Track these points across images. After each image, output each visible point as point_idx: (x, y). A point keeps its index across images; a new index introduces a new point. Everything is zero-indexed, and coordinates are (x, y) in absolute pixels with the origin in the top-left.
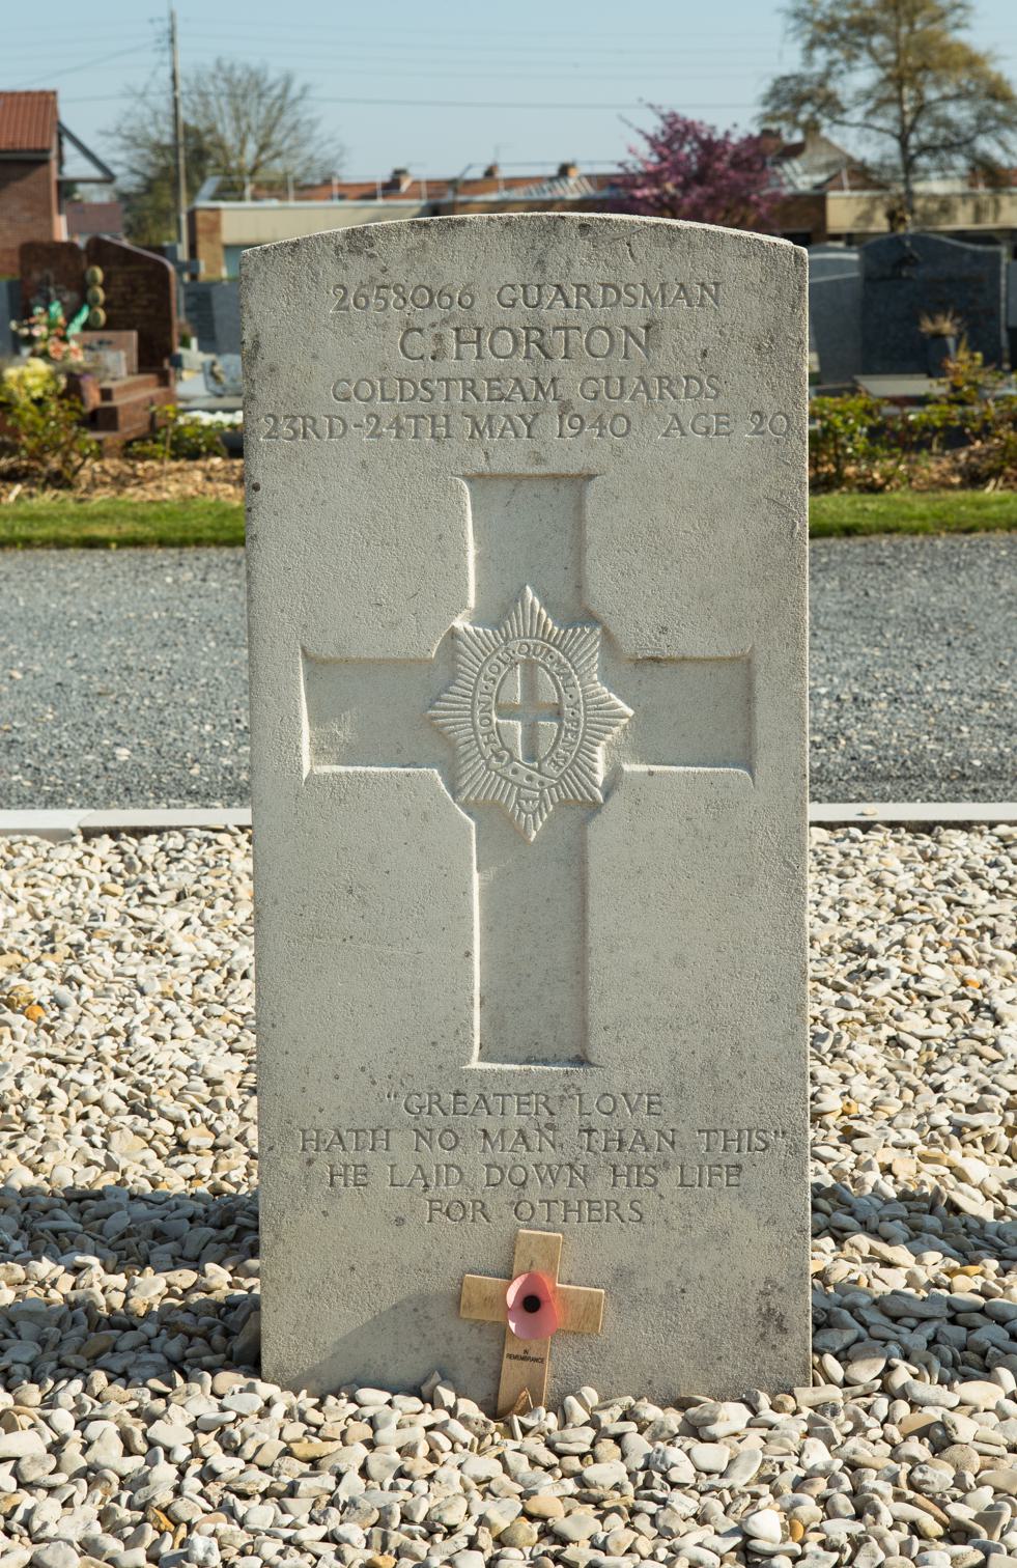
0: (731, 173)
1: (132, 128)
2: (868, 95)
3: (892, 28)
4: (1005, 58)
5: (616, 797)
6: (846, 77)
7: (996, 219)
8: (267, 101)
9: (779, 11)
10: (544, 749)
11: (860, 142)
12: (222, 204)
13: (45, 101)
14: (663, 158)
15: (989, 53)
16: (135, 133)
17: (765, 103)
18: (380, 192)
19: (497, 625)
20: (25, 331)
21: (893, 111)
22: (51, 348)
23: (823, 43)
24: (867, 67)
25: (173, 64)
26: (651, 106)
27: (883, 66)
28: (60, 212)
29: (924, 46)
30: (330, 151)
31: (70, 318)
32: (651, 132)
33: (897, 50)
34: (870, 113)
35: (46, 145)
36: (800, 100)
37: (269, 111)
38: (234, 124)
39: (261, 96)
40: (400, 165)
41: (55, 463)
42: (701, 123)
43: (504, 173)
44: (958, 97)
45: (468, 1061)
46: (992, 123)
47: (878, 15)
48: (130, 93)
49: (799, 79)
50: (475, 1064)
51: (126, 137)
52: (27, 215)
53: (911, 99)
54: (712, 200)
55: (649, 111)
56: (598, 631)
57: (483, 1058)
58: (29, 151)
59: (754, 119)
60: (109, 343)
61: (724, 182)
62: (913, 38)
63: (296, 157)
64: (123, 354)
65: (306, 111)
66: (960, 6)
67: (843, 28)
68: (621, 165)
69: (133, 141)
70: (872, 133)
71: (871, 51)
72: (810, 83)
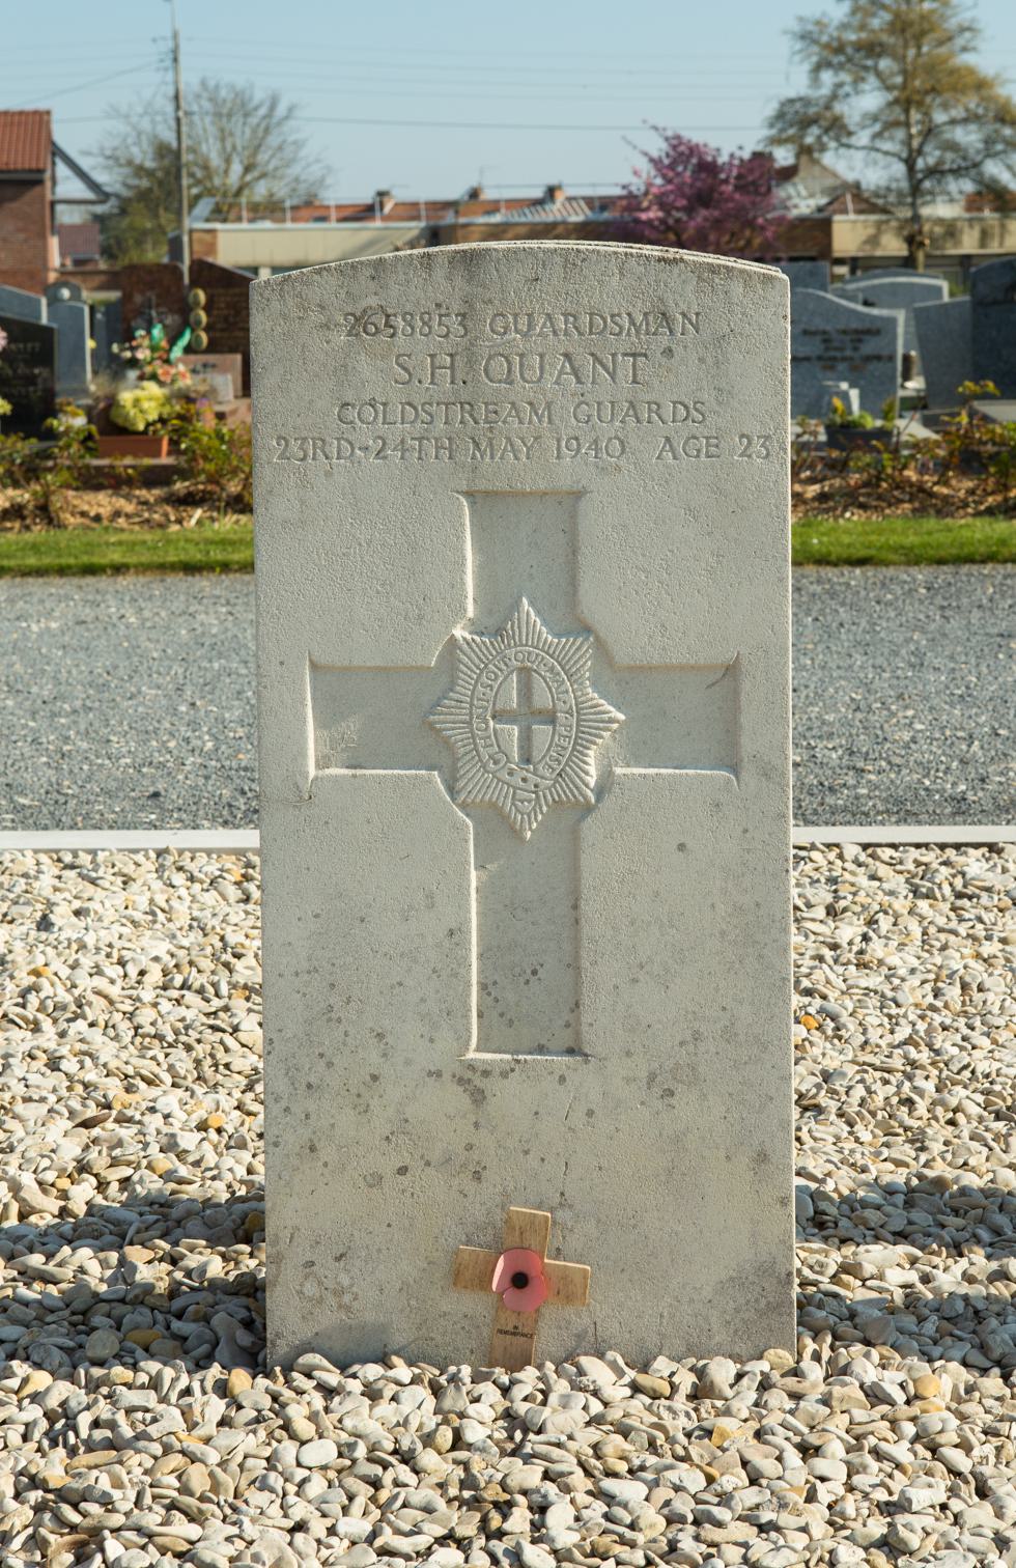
0: (737, 196)
1: (115, 149)
2: (875, 118)
3: (900, 51)
5: (609, 801)
6: (853, 100)
7: (1001, 244)
8: (253, 121)
9: (785, 32)
11: (867, 165)
12: (218, 226)
13: (38, 122)
14: (669, 181)
15: (997, 76)
17: (771, 126)
20: (128, 354)
21: (900, 134)
22: (160, 371)
23: (829, 65)
25: (176, 83)
26: (655, 128)
27: (889, 88)
28: (53, 233)
29: (931, 69)
30: (316, 171)
31: (172, 341)
32: (655, 154)
33: (904, 72)
34: (877, 136)
35: (41, 166)
36: (806, 123)
37: (254, 131)
38: (218, 145)
39: (246, 115)
40: (383, 187)
41: (234, 487)
42: (705, 145)
43: (488, 195)
44: (965, 121)
46: (999, 147)
47: (885, 38)
48: (114, 112)
51: (108, 158)
52: (21, 236)
53: (918, 122)
54: (717, 223)
55: (653, 132)
58: (24, 171)
60: (214, 366)
61: (731, 205)
62: (920, 61)
63: (281, 178)
64: (230, 377)
66: (969, 29)
67: (849, 50)
68: (624, 187)
69: (113, 159)
70: (879, 156)
71: (879, 74)
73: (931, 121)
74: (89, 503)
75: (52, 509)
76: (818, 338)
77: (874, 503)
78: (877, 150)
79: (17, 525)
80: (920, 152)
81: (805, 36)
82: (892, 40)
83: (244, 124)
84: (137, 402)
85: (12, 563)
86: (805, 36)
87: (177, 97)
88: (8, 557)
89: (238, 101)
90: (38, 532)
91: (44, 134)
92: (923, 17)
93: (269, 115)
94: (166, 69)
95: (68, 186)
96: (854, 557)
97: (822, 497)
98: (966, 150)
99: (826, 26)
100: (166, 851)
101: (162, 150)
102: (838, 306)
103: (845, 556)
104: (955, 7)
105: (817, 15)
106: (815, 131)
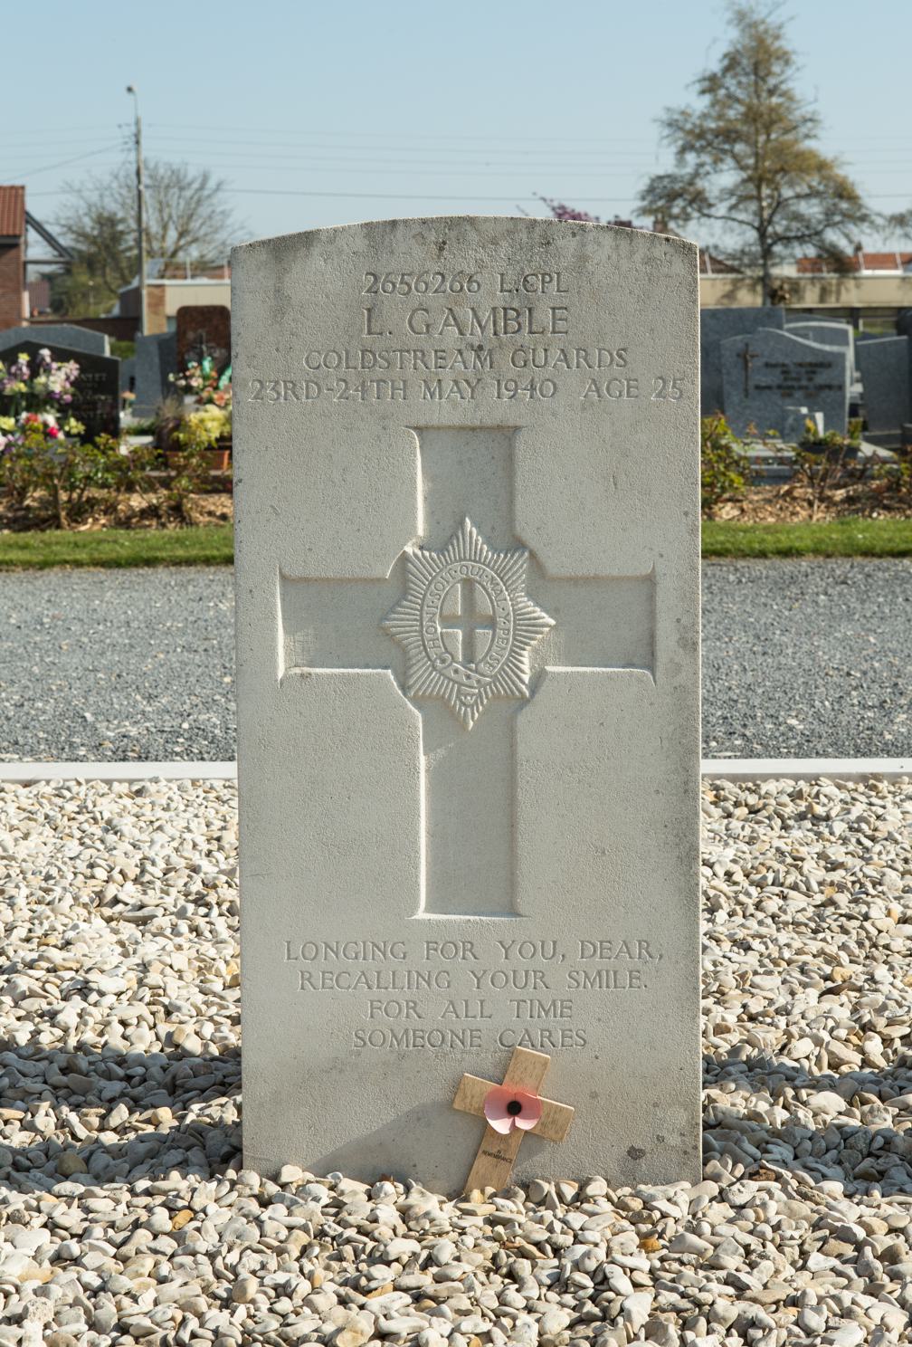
2: (732, 193)
6: (714, 177)
8: (188, 193)
9: (655, 121)
11: (725, 232)
12: (166, 282)
13: (16, 193)
15: (836, 158)
16: (71, 222)
17: (643, 198)
19: (442, 550)
20: (183, 382)
21: (753, 206)
26: (544, 200)
27: (743, 168)
29: (780, 151)
33: (756, 155)
35: (17, 232)
36: (672, 196)
37: (188, 203)
38: (157, 214)
39: (182, 189)
44: (807, 196)
46: (837, 218)
47: (739, 126)
48: (69, 188)
49: (672, 178)
50: (421, 914)
51: (63, 226)
55: (541, 202)
56: (526, 554)
57: (427, 910)
59: (633, 212)
65: (222, 202)
66: (811, 120)
70: (735, 224)
71: (735, 157)
72: (681, 181)
73: (780, 195)
74: (214, 504)
75: (184, 508)
76: (778, 370)
77: (897, 505)
78: (734, 220)
79: (154, 523)
80: (770, 222)
81: (671, 124)
82: (745, 128)
83: (179, 197)
85: (164, 554)
86: (671, 124)
88: (159, 549)
89: (174, 178)
90: (173, 529)
91: (19, 201)
92: (772, 110)
93: (202, 188)
94: (129, 150)
95: (36, 249)
96: (896, 550)
97: (849, 500)
98: (809, 221)
99: (690, 115)
101: (106, 222)
102: (795, 342)
103: (887, 549)
104: (799, 102)
105: (683, 107)
106: (680, 203)
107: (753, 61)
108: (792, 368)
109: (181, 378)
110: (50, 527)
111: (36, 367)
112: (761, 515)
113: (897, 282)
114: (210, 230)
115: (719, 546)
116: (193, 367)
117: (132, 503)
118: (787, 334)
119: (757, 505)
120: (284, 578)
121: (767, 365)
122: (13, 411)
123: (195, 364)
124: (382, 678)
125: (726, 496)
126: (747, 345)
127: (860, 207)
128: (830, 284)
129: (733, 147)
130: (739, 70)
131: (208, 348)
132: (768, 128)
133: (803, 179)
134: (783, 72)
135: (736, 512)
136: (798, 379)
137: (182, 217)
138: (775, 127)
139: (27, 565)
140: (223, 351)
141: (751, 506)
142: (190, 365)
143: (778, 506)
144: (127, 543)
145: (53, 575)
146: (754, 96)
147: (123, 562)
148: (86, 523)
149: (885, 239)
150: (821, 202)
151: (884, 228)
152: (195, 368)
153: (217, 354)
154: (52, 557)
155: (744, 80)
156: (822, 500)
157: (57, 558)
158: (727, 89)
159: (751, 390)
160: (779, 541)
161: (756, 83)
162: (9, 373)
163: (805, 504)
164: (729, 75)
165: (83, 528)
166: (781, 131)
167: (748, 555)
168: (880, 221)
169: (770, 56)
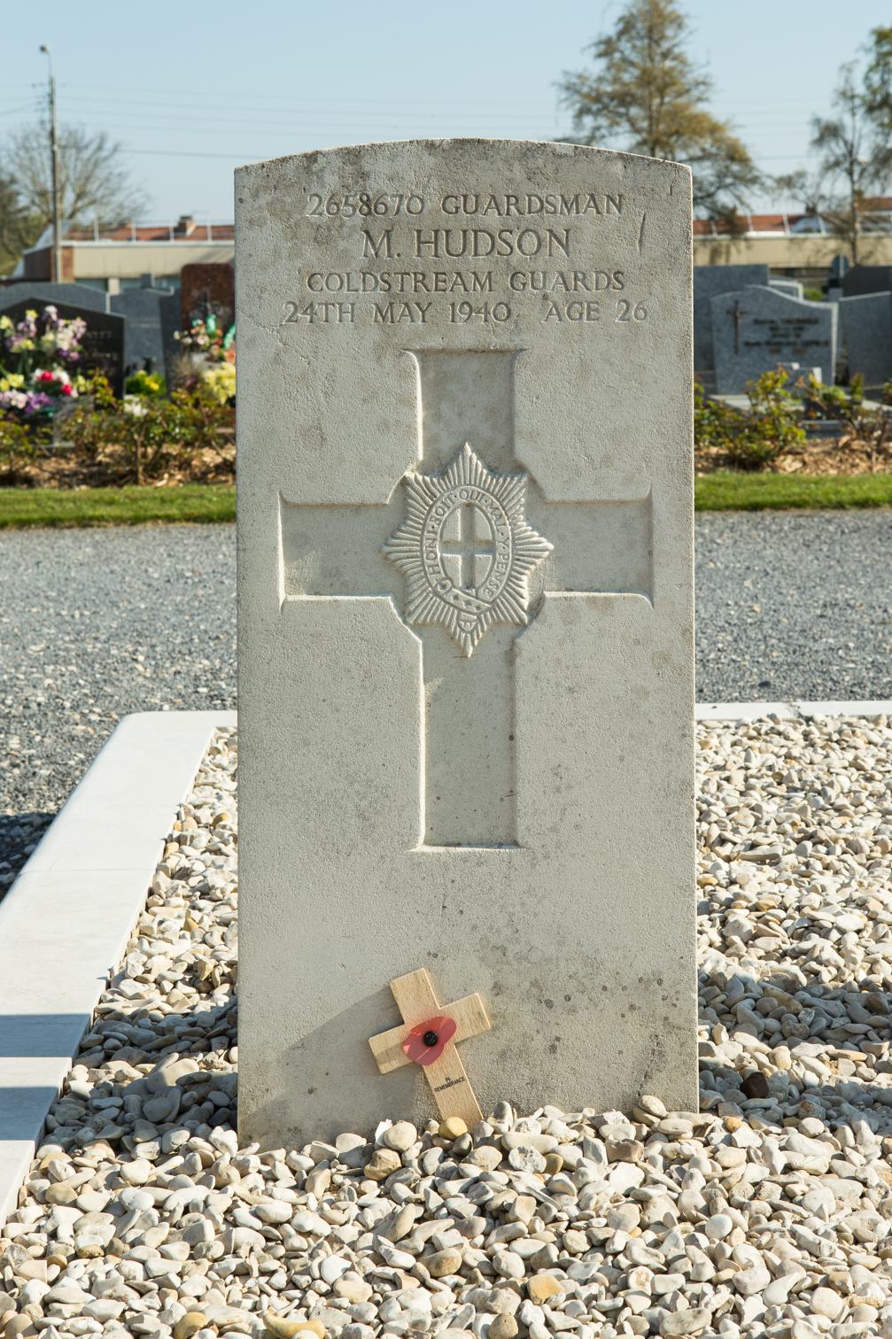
4: (741, 126)
8: (86, 154)
9: (553, 84)
10: (479, 581)
12: (74, 243)
18: (172, 234)
20: (189, 340)
24: (625, 132)
27: (637, 131)
29: (675, 113)
33: (650, 118)
37: (85, 165)
39: (79, 149)
40: (186, 213)
45: (408, 843)
46: (729, 180)
47: (634, 90)
56: (525, 479)
57: (427, 843)
62: (664, 108)
63: (107, 204)
65: (120, 163)
66: (704, 83)
71: (632, 122)
76: (767, 327)
81: (569, 88)
83: (77, 159)
84: (219, 380)
86: (569, 88)
87: (52, 134)
92: (667, 73)
93: (100, 148)
94: (43, 110)
99: (587, 79)
100: (204, 760)
105: (580, 70)
107: (647, 24)
108: (781, 325)
109: (186, 336)
110: (126, 483)
111: (43, 324)
112: (823, 467)
113: (786, 243)
114: (107, 192)
115: (797, 498)
116: (198, 325)
117: (206, 459)
118: (775, 291)
119: (817, 457)
120: (285, 503)
121: (756, 322)
122: (20, 369)
123: (200, 322)
124: (381, 605)
125: (787, 449)
126: (737, 302)
127: (751, 169)
128: (720, 245)
129: (628, 109)
130: (633, 33)
131: (213, 306)
132: (662, 92)
133: (696, 142)
134: (676, 35)
135: (798, 465)
136: (786, 336)
137: (80, 178)
138: (668, 91)
139: (119, 521)
140: (228, 309)
141: (812, 459)
142: (194, 323)
143: (838, 458)
144: (215, 499)
145: (149, 531)
146: (648, 60)
147: (215, 517)
148: (162, 479)
149: (774, 201)
150: (713, 165)
151: (773, 189)
152: (200, 326)
153: (221, 312)
154: (142, 513)
155: (638, 43)
156: (879, 452)
157: (149, 513)
158: (622, 52)
159: (741, 347)
160: (853, 493)
161: (650, 46)
162: (17, 331)
163: (864, 456)
164: (624, 38)
165: (160, 484)
166: (673, 95)
167: (826, 507)
168: (769, 183)
169: (664, 20)
